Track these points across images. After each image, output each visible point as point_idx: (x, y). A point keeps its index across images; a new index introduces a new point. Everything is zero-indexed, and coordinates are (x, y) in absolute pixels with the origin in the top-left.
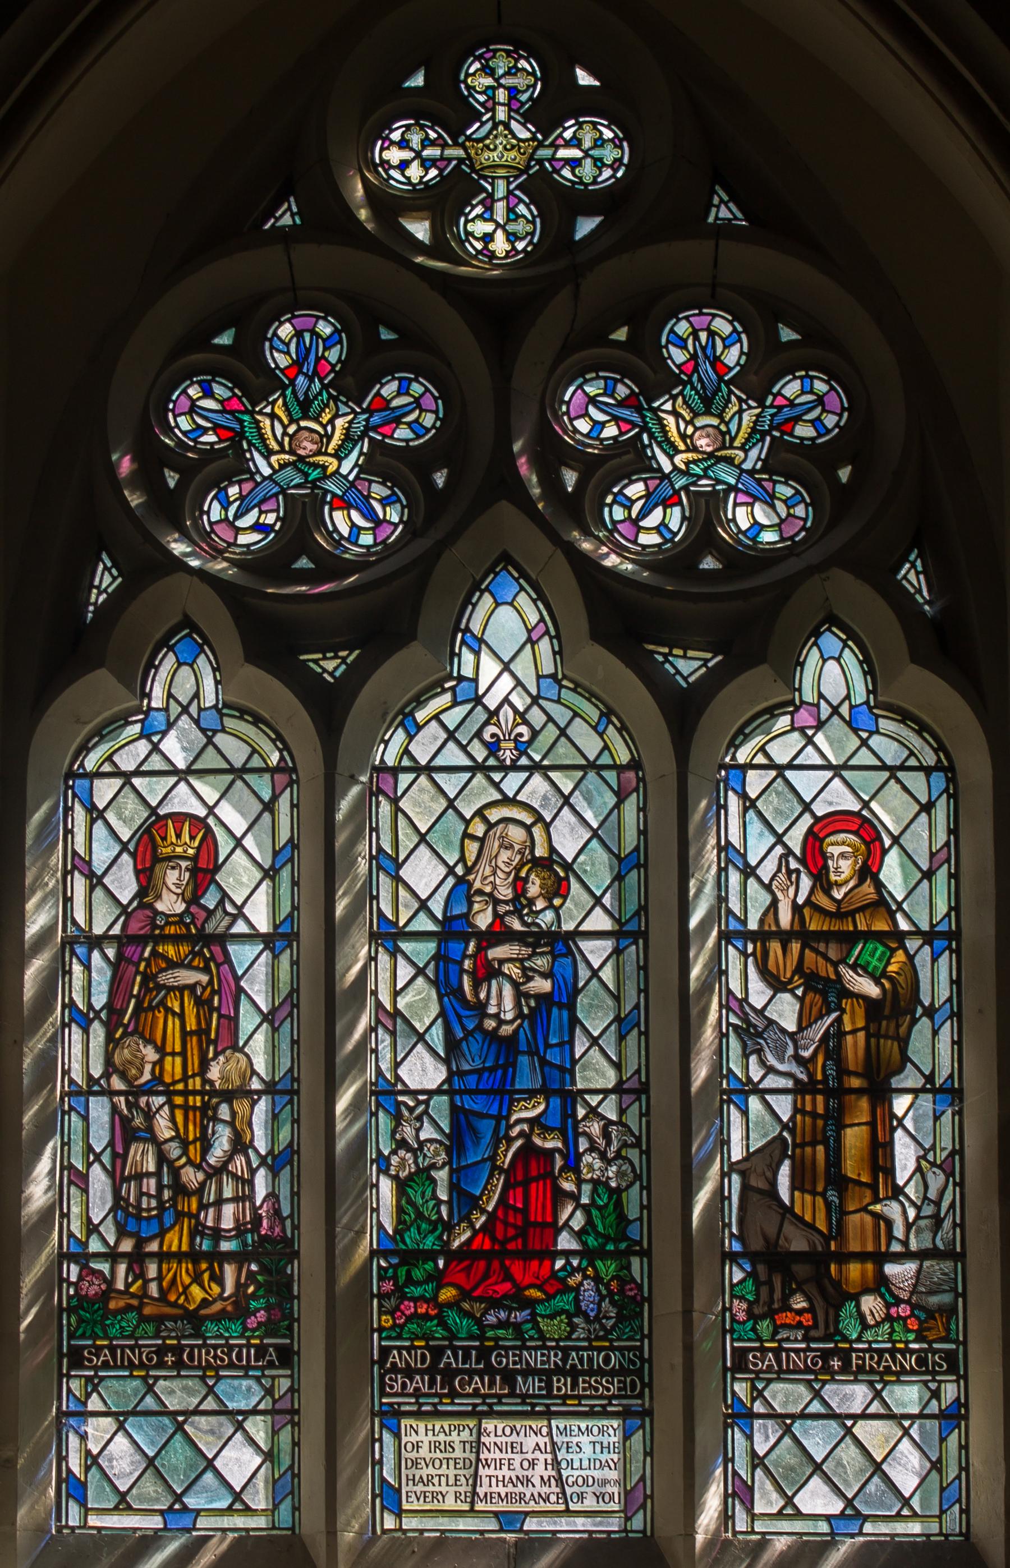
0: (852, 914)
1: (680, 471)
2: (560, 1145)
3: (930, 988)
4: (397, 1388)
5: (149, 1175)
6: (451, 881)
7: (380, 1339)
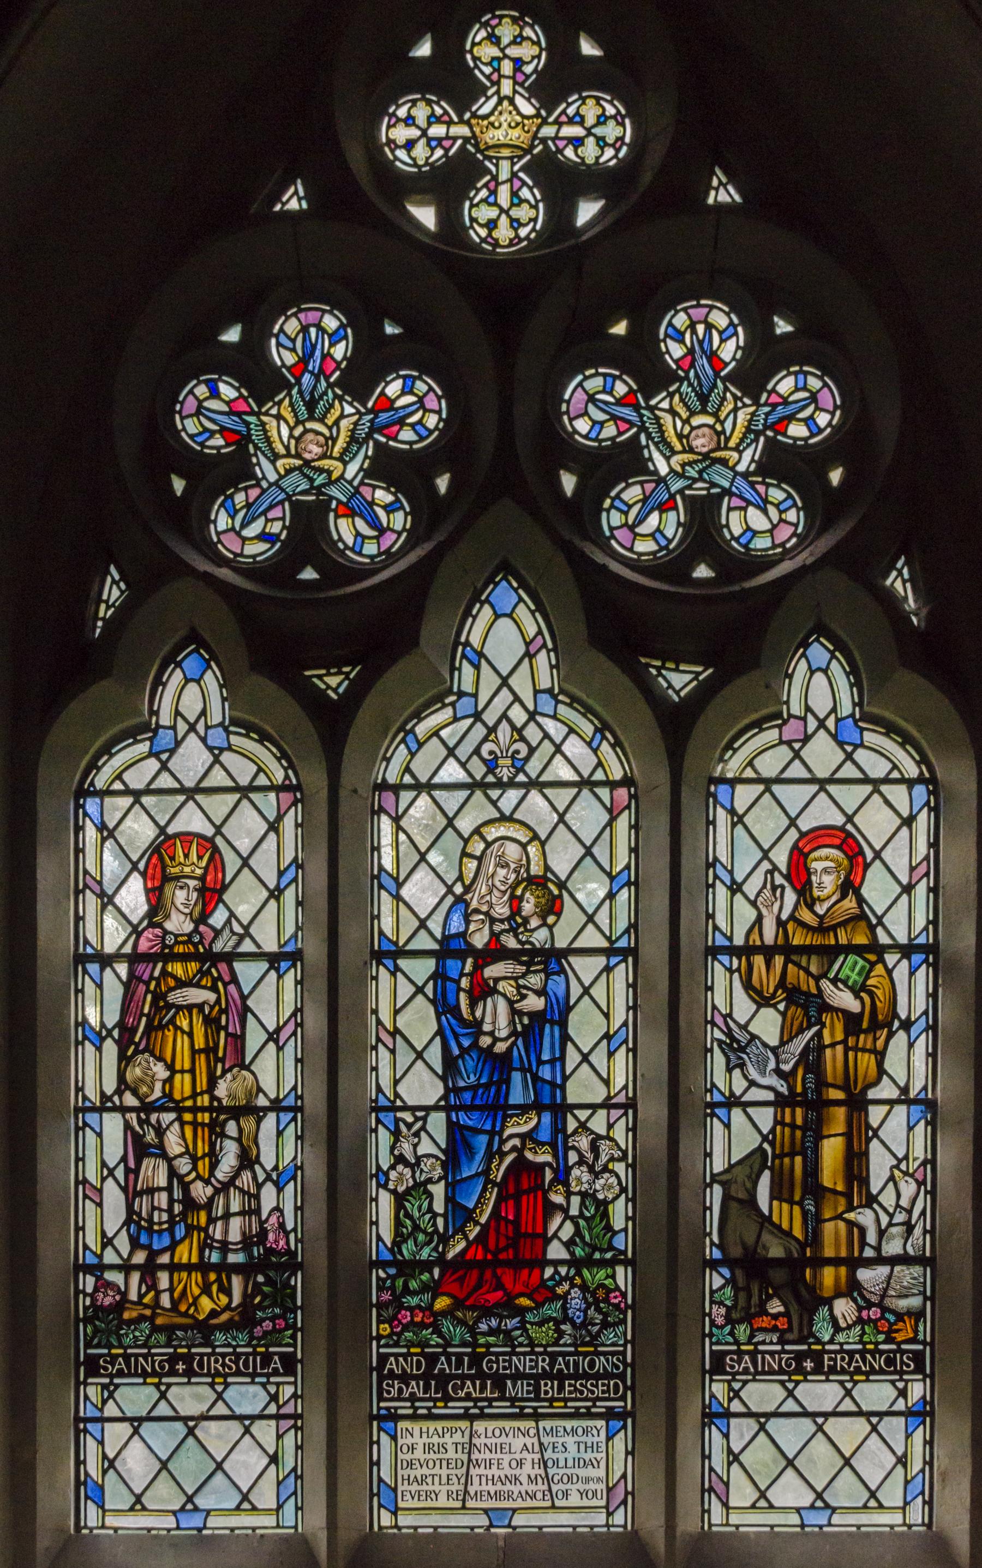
0: (834, 928)
1: (676, 473)
2: (548, 1158)
3: (906, 1000)
4: (394, 1393)
5: (160, 1189)
6: (450, 900)
7: (379, 1347)
